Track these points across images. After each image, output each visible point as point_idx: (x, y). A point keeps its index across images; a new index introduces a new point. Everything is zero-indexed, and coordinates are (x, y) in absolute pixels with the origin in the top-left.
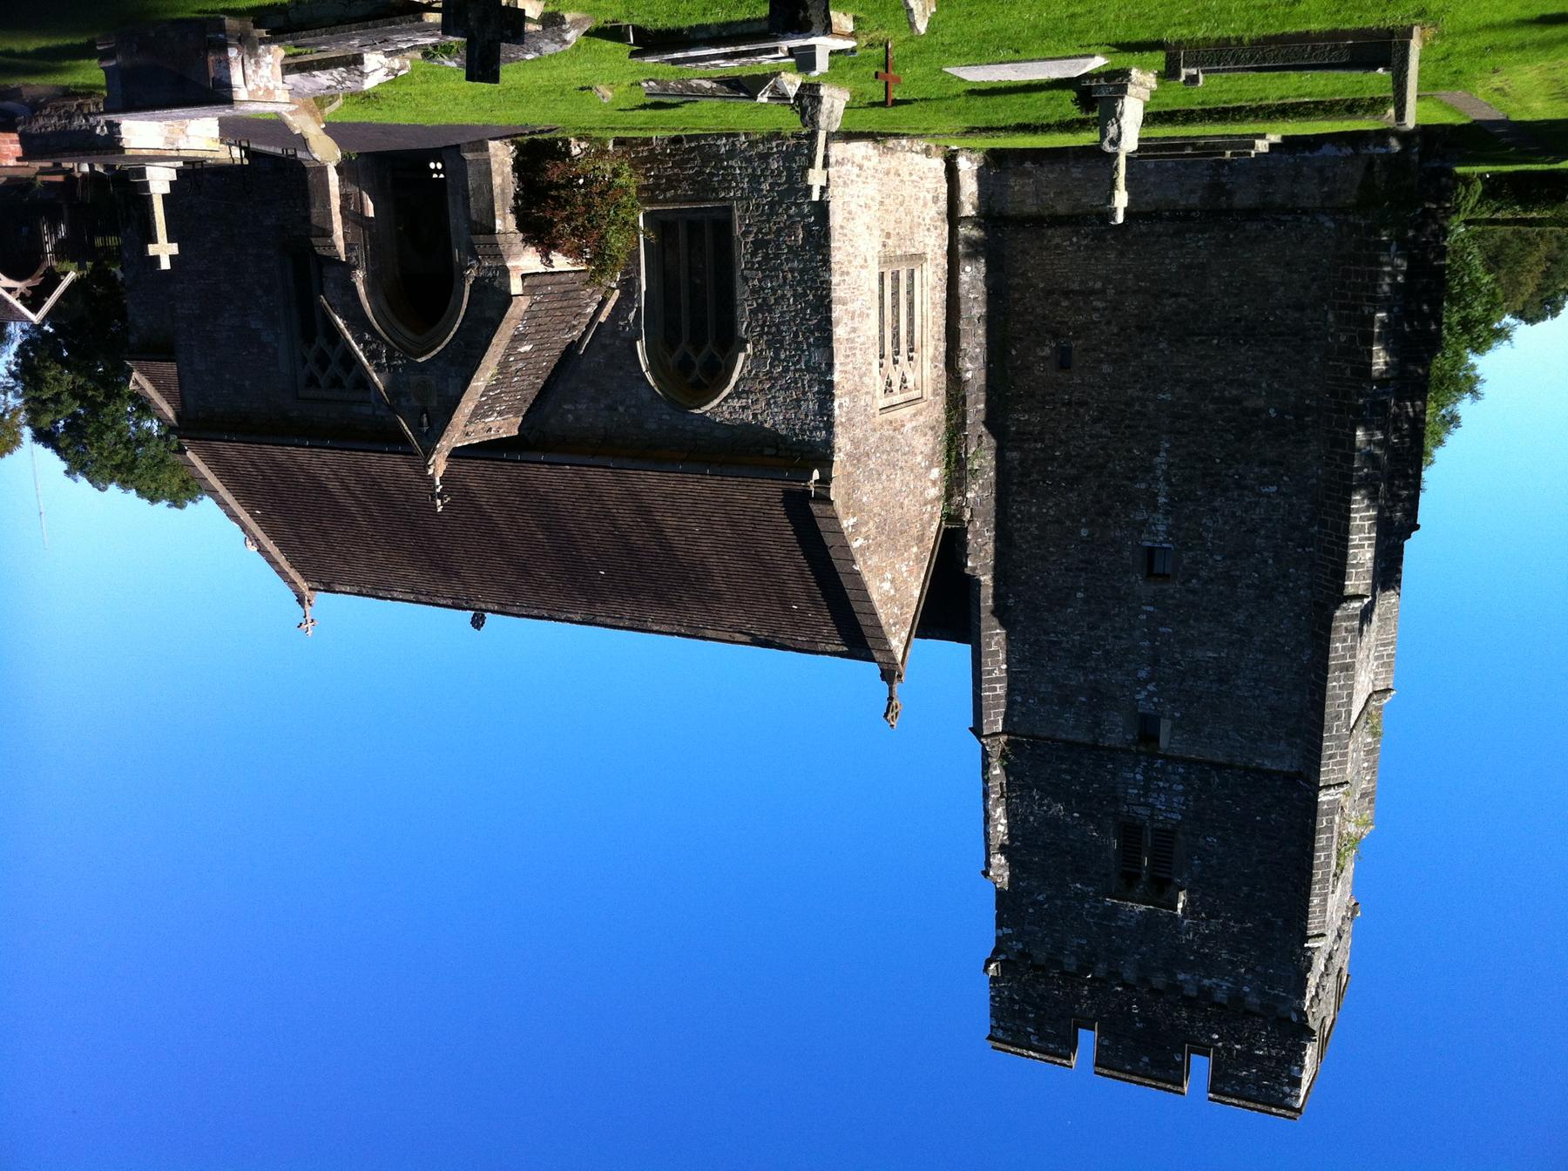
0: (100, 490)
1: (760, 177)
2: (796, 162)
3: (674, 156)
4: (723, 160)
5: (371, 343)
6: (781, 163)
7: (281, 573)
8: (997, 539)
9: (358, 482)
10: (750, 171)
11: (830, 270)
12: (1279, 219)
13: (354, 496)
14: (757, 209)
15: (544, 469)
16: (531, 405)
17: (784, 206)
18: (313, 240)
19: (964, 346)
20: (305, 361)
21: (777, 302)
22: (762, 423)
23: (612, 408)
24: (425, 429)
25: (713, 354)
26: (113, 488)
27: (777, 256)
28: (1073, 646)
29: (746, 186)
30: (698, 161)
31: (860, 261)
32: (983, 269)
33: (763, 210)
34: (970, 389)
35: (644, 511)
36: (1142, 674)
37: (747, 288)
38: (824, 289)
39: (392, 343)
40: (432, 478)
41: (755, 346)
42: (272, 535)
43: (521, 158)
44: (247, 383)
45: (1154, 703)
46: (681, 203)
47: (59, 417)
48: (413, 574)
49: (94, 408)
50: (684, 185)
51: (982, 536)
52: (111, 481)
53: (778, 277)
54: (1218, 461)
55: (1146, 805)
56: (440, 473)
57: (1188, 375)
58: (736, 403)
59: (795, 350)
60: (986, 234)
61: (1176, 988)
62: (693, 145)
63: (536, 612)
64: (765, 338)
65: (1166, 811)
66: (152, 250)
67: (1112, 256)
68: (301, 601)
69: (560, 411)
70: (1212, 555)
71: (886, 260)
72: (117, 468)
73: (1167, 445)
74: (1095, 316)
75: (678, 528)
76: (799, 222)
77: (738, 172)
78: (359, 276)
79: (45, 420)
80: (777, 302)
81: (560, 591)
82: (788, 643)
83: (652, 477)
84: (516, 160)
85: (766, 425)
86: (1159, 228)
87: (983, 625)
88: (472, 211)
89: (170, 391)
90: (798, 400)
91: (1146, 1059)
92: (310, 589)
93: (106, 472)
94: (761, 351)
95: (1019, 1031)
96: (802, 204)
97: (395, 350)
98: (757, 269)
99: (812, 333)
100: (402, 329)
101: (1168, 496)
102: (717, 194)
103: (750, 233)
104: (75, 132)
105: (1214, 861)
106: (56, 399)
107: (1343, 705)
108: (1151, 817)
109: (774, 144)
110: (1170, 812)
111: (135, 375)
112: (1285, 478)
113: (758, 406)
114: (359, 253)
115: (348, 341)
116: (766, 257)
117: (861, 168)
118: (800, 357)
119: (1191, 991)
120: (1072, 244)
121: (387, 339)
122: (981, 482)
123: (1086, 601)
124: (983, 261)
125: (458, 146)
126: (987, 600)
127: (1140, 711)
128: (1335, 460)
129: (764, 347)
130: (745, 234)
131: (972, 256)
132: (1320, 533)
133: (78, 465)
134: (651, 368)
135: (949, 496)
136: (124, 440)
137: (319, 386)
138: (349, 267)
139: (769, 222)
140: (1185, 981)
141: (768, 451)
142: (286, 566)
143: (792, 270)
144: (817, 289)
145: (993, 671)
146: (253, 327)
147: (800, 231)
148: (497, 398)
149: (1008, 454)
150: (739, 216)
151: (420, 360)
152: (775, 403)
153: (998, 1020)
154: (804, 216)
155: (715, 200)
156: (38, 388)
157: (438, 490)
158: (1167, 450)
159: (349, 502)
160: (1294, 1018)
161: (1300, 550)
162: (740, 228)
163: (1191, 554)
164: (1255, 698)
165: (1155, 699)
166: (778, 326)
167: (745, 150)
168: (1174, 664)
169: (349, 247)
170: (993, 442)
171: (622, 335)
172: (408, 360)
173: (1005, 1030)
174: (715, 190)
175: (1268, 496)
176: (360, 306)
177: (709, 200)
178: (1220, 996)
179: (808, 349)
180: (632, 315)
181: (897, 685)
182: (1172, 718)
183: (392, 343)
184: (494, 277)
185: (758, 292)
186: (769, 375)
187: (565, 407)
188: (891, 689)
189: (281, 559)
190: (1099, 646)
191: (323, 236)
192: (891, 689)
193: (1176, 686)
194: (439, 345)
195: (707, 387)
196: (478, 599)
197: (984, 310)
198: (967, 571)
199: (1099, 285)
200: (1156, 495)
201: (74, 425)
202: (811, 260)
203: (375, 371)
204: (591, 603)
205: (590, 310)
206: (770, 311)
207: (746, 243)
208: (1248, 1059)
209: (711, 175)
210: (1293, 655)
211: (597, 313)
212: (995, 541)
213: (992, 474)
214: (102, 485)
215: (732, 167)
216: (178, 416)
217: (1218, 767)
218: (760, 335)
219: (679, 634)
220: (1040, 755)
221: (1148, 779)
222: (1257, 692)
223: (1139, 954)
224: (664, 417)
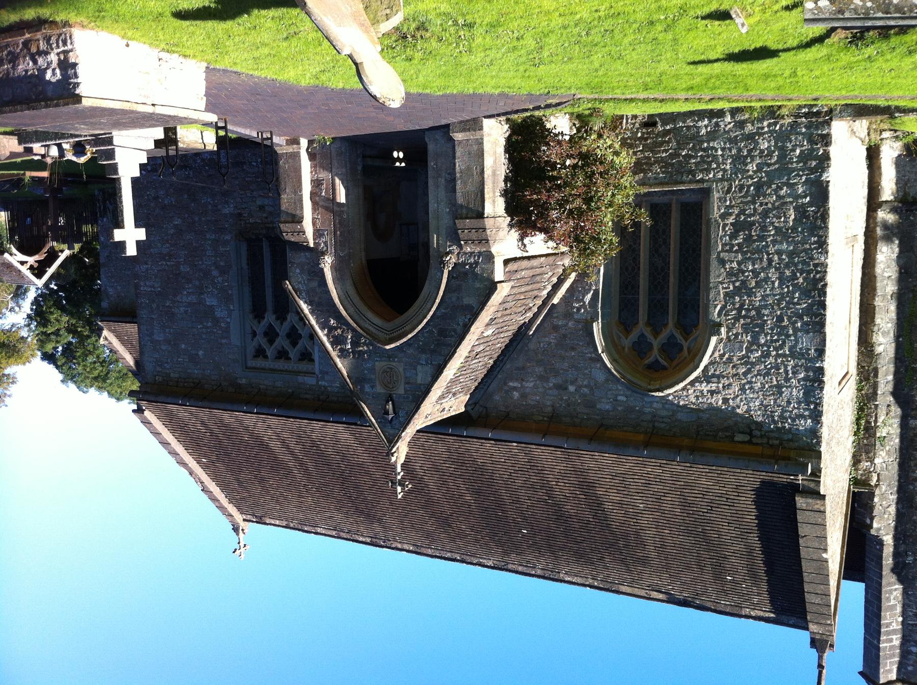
0: (84, 392)
1: (746, 157)
2: (791, 142)
3: (646, 139)
4: (702, 142)
5: (336, 329)
6: (773, 143)
7: (221, 508)
8: (899, 501)
9: (298, 443)
10: (734, 152)
11: (827, 253)
13: (292, 453)
14: (740, 191)
15: (488, 445)
16: (479, 384)
17: (774, 186)
18: (281, 225)
19: (878, 321)
20: (254, 334)
21: (758, 285)
22: (734, 408)
23: (562, 387)
24: (390, 417)
25: (673, 335)
26: (92, 391)
27: (762, 238)
29: (728, 167)
30: (674, 144)
32: (897, 250)
33: (748, 191)
34: (882, 361)
35: (586, 486)
37: (723, 270)
38: (818, 272)
39: (358, 329)
40: (394, 467)
41: (729, 329)
42: (215, 478)
43: (514, 138)
44: (201, 353)
46: (651, 186)
47: (58, 345)
48: (338, 516)
49: (82, 339)
50: (657, 168)
51: (886, 499)
52: (91, 386)
53: (761, 260)
56: (402, 460)
58: (704, 387)
59: (779, 334)
60: (900, 218)
62: (668, 127)
63: (449, 555)
64: (742, 321)
66: (118, 235)
68: (236, 529)
69: (506, 388)
72: (96, 379)
75: (620, 503)
76: (791, 203)
77: (720, 152)
78: (327, 264)
79: (49, 348)
80: (758, 285)
81: (477, 541)
82: (709, 605)
83: (607, 459)
84: (508, 140)
85: (739, 411)
87: (884, 582)
88: (459, 195)
89: (132, 344)
90: (779, 387)
92: (244, 520)
93: (88, 381)
94: (736, 335)
96: (796, 184)
97: (361, 336)
98: (736, 252)
99: (801, 317)
100: (370, 315)
102: (694, 176)
103: (731, 214)
104: (20, 79)
106: (57, 333)
109: (765, 123)
111: (105, 333)
113: (731, 391)
114: (328, 238)
115: (312, 326)
116: (748, 239)
118: (784, 343)
121: (355, 325)
122: (887, 448)
124: (897, 242)
125: (447, 127)
126: (888, 561)
129: (740, 331)
130: (724, 216)
131: (888, 239)
133: (70, 377)
134: (606, 349)
135: (856, 461)
136: (101, 360)
137: (266, 357)
138: (316, 254)
139: (754, 203)
141: (739, 437)
142: (224, 501)
143: (779, 253)
144: (809, 272)
145: (890, 624)
146: (208, 303)
147: (792, 212)
149: (911, 422)
150: (720, 199)
151: (388, 347)
152: (751, 388)
154: (797, 197)
155: (690, 182)
156: (45, 326)
157: (399, 477)
159: (287, 458)
162: (719, 209)
166: (758, 310)
167: (730, 130)
169: (318, 234)
170: (899, 411)
171: (576, 317)
172: (375, 347)
174: (692, 172)
176: (328, 292)
177: (682, 183)
179: (795, 334)
180: (588, 297)
181: (827, 654)
183: (358, 329)
184: (476, 263)
185: (736, 275)
186: (745, 360)
187: (511, 384)
188: (820, 658)
189: (221, 497)
191: (293, 222)
192: (820, 658)
194: (410, 332)
195: (664, 368)
196: (395, 541)
197: (896, 288)
198: (873, 532)
201: (68, 350)
202: (803, 242)
203: (339, 356)
204: (506, 553)
205: (545, 293)
206: (750, 293)
207: (725, 225)
209: (688, 157)
211: (551, 295)
212: (897, 503)
213: (897, 441)
214: (85, 389)
215: (713, 148)
216: (137, 363)
218: (737, 319)
219: (591, 586)
224: (620, 398)
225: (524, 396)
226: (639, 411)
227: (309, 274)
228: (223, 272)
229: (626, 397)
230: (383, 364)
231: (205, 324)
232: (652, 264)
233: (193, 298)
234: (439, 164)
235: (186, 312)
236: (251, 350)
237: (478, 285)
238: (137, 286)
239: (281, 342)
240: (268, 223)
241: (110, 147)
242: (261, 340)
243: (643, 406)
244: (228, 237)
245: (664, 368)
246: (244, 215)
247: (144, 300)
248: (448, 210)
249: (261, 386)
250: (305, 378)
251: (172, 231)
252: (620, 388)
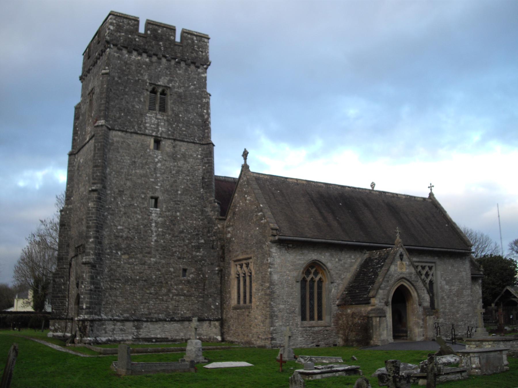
28: (182, 175)
31: (259, 308)
36: (159, 165)
44: (450, 268)
45: (155, 154)
55: (158, 119)
61: (150, 56)
71: (249, 308)
74: (175, 287)
86: (156, 315)
95: (200, 41)
101: (151, 226)
105: (137, 99)
107: (97, 153)
108: (156, 114)
117: (258, 337)
119: (144, 55)
120: (183, 311)
123: (178, 190)
127: (160, 152)
148: (378, 263)
153: (206, 45)
158: (152, 241)
163: (144, 206)
164: (124, 156)
165: (155, 156)
173: (204, 42)
175: (120, 225)
178: (135, 53)
182: (150, 149)
190: (173, 175)
193: (149, 160)
199: (174, 297)
208: (128, 32)
217: (136, 133)
225: (350, 257)
228: (443, 298)
232: (313, 301)
233: (453, 288)
235: (455, 283)
238: (471, 292)
239: (424, 272)
241: (43, 326)
242: (430, 273)
244: (441, 310)
245: (310, 267)
247: (469, 287)
251: (460, 312)
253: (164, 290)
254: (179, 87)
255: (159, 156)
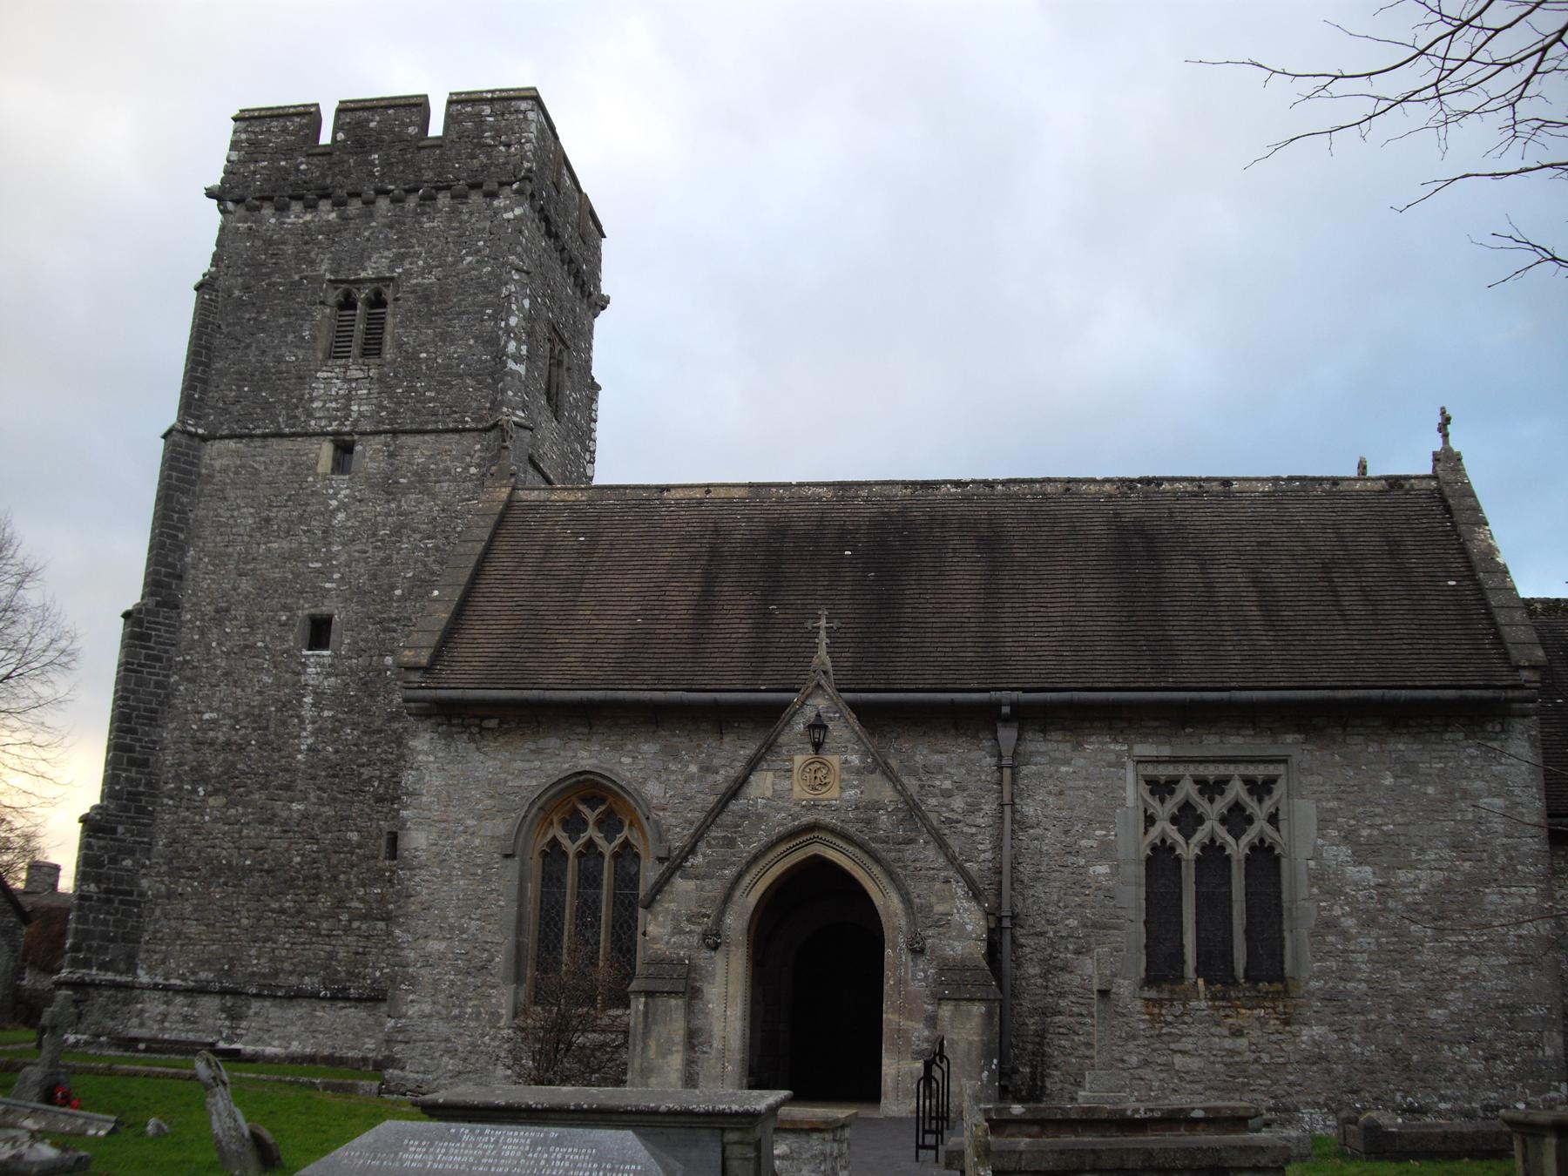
12: (183, 980)
20: (1273, 819)
36: (341, 516)
44: (1389, 781)
45: (332, 488)
54: (253, 742)
57: (276, 829)
61: (339, 204)
65: (331, 378)
67: (341, 955)
70: (266, 647)
73: (299, 757)
74: (361, 892)
86: (293, 980)
91: (372, 125)
110: (328, 378)
112: (194, 727)
119: (325, 205)
120: (381, 969)
128: (142, 747)
132: (167, 676)
140: (329, 212)
146: (1368, 869)
158: (300, 751)
160: (230, 205)
161: (188, 658)
164: (239, 507)
165: (331, 491)
168: (308, 531)
178: (297, 207)
200: (313, 705)
210: (202, 555)
220: (456, 412)
221: (347, 407)
222: (236, 513)
223: (372, 227)
226: (606, 746)
227: (948, 922)
229: (620, 762)
230: (828, 795)
231: (1375, 833)
234: (720, 1066)
235: (1422, 851)
236: (1279, 790)
237: (673, 906)
240: (1225, 1007)
243: (599, 752)
246: (1278, 1022)
248: (710, 1006)
249: (1252, 733)
250: (1155, 754)
251: (1451, 996)
252: (628, 774)
253: (324, 902)
254: (428, 269)
255: (343, 488)
